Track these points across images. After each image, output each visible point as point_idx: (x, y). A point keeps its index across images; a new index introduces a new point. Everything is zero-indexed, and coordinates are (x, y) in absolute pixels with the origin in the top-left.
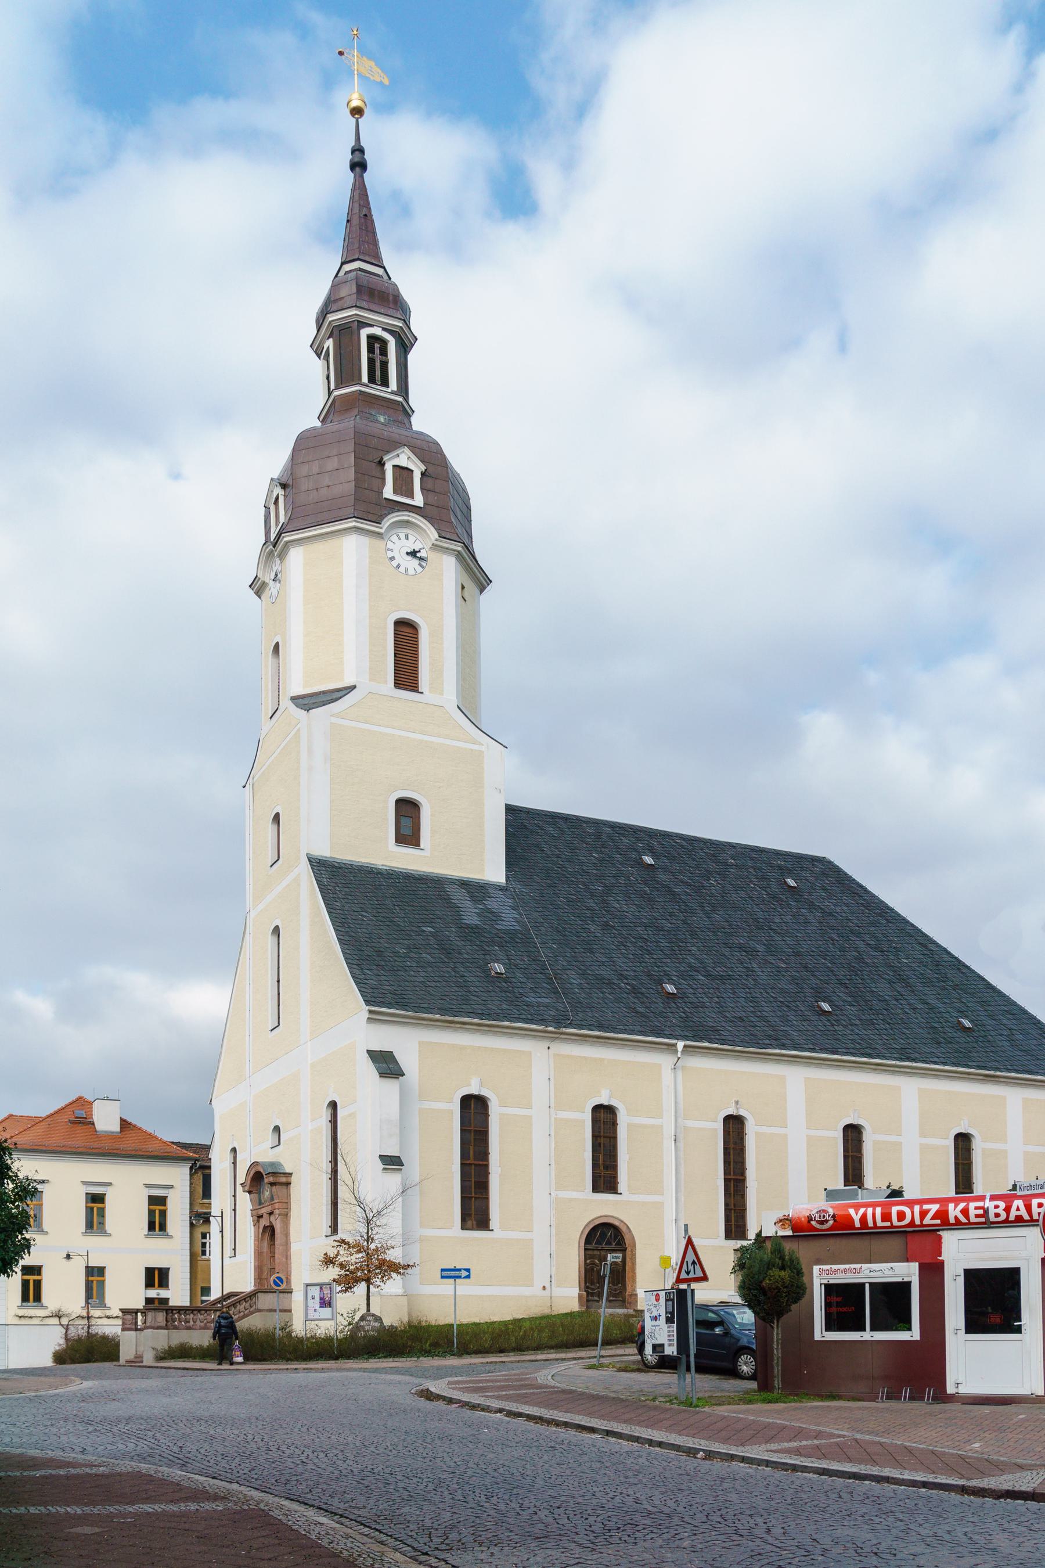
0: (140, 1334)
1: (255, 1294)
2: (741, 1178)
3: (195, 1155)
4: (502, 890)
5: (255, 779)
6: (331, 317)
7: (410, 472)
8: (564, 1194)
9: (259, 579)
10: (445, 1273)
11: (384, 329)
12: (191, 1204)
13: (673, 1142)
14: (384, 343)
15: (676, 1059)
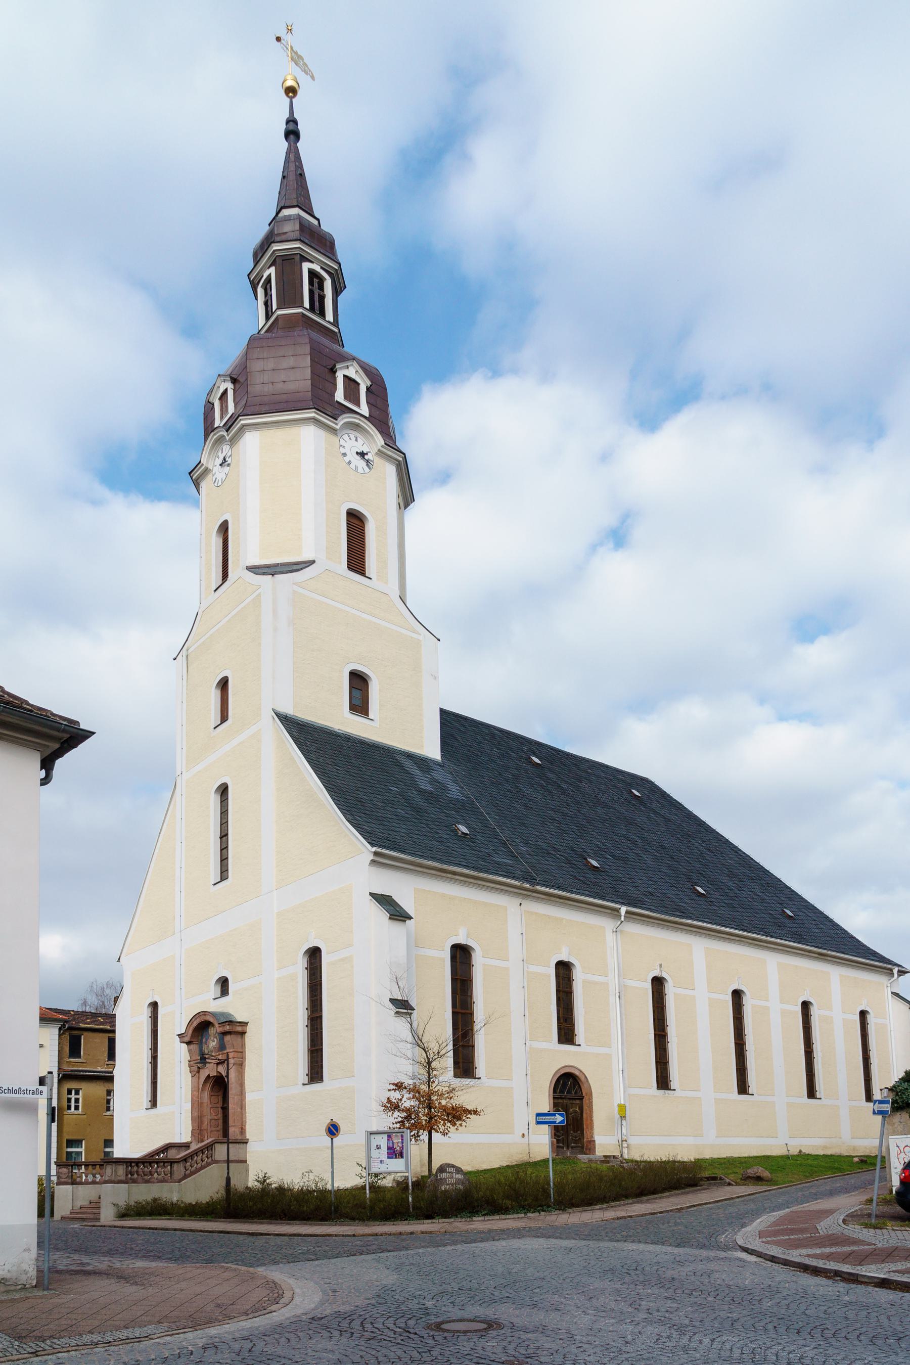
0: (77, 1187)
1: (212, 1145)
2: (663, 1034)
3: (64, 1017)
4: (440, 765)
5: (190, 651)
6: (276, 247)
7: (357, 385)
8: (536, 1045)
9: (203, 465)
10: (540, 1119)
11: (322, 268)
12: (59, 1063)
13: (618, 999)
14: (321, 281)
15: (619, 922)
